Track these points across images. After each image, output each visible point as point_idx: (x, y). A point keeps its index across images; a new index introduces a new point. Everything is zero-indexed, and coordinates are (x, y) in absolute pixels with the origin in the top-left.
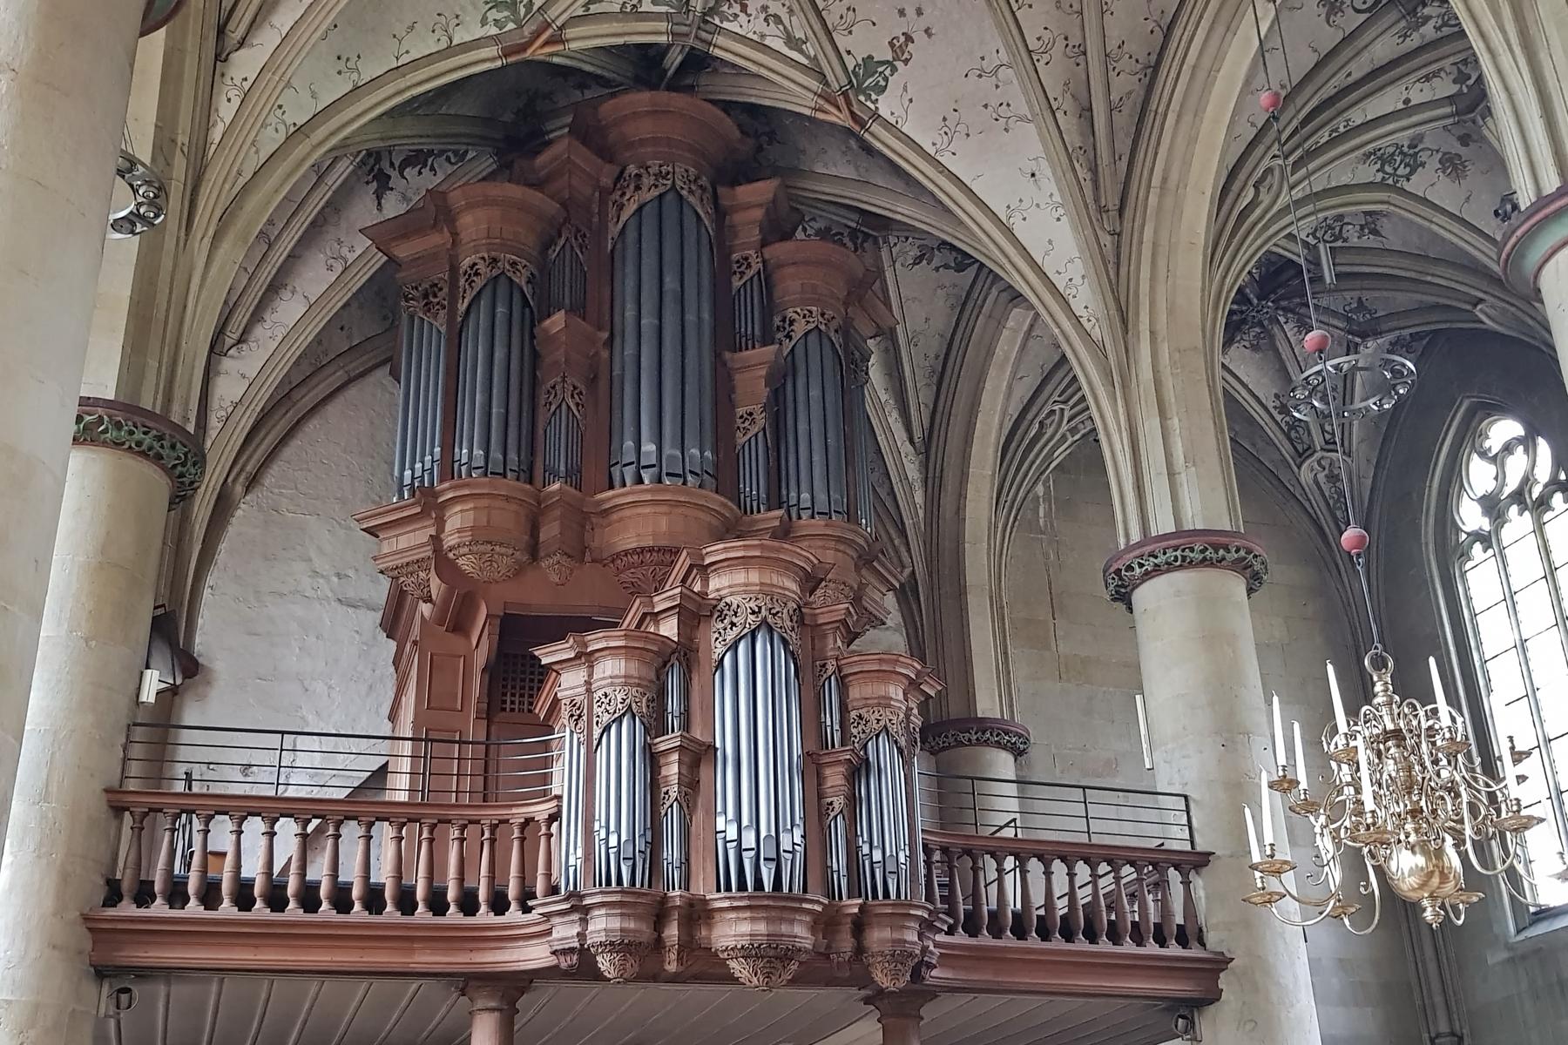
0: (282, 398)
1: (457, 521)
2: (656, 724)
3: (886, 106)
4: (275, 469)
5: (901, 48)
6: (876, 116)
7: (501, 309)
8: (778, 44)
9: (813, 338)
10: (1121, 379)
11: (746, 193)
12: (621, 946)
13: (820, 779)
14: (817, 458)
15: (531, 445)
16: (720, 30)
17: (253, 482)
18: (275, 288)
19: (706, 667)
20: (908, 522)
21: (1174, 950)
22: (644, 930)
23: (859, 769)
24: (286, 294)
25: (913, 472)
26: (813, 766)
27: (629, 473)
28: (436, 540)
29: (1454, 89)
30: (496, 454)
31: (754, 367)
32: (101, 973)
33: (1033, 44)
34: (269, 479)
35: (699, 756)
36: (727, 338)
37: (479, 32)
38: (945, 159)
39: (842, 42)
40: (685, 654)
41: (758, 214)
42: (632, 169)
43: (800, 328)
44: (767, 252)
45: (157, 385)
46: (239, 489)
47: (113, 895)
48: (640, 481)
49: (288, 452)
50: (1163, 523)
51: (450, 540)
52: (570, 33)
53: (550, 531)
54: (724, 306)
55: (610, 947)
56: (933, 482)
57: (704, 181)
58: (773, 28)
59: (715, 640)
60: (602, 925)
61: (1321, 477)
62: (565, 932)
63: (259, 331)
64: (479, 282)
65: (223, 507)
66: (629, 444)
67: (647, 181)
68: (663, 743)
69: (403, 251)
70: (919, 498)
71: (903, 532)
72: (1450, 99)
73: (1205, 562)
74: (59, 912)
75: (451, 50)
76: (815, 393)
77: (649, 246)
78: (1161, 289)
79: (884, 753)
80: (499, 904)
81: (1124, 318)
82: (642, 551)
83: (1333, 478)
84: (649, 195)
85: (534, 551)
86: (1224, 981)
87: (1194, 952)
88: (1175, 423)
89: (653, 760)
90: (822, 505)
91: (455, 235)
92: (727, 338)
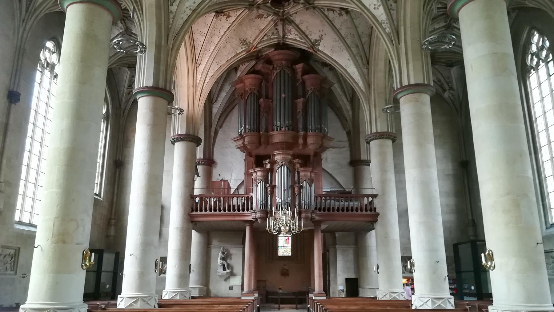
0: (224, 111)
1: (247, 139)
2: (266, 182)
3: (320, 48)
4: (225, 124)
5: (321, 37)
6: (319, 50)
7: (252, 98)
8: (299, 39)
9: (312, 95)
10: (368, 101)
11: (298, 66)
12: (261, 218)
13: (294, 189)
14: (313, 118)
15: (259, 124)
16: (287, 38)
17: (221, 127)
18: (220, 90)
19: (275, 171)
20: (348, 119)
21: (369, 212)
22: (265, 215)
23: (301, 187)
24: (222, 92)
25: (349, 107)
26: (292, 187)
27: (275, 128)
28: (243, 143)
29: (445, 24)
30: (252, 127)
31: (300, 101)
32: (192, 222)
33: (344, 36)
34: (224, 126)
35: (273, 187)
36: (295, 96)
37: (242, 50)
38: (333, 57)
39: (310, 37)
40: (272, 170)
41: (301, 70)
42: (275, 66)
43: (310, 92)
44: (303, 77)
45: (230, 59)
46: (219, 128)
47: (192, 211)
48: (277, 130)
49: (227, 120)
50: (374, 131)
51: (246, 143)
52: (258, 46)
53: (262, 140)
54: (294, 89)
55: (259, 218)
56: (353, 109)
57: (290, 65)
58: (297, 36)
59: (276, 167)
60: (258, 215)
61: (450, 95)
62: (254, 215)
63: (219, 99)
64: (248, 93)
65: (216, 133)
66: (275, 122)
67: (278, 68)
68: (268, 185)
69: (237, 87)
70: (351, 113)
71: (347, 121)
72: (444, 27)
73: (380, 138)
74: (184, 214)
75: (237, 55)
76: (313, 105)
77: (278, 81)
78: (376, 80)
79: (305, 184)
80: (243, 210)
81: (369, 86)
82: (277, 143)
83: (453, 95)
84: (278, 71)
85: (260, 144)
86: (378, 218)
87: (373, 213)
88: (377, 109)
89: (266, 188)
90: (313, 128)
91: (245, 84)
92: (295, 96)
